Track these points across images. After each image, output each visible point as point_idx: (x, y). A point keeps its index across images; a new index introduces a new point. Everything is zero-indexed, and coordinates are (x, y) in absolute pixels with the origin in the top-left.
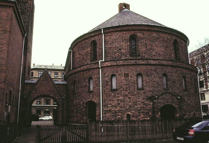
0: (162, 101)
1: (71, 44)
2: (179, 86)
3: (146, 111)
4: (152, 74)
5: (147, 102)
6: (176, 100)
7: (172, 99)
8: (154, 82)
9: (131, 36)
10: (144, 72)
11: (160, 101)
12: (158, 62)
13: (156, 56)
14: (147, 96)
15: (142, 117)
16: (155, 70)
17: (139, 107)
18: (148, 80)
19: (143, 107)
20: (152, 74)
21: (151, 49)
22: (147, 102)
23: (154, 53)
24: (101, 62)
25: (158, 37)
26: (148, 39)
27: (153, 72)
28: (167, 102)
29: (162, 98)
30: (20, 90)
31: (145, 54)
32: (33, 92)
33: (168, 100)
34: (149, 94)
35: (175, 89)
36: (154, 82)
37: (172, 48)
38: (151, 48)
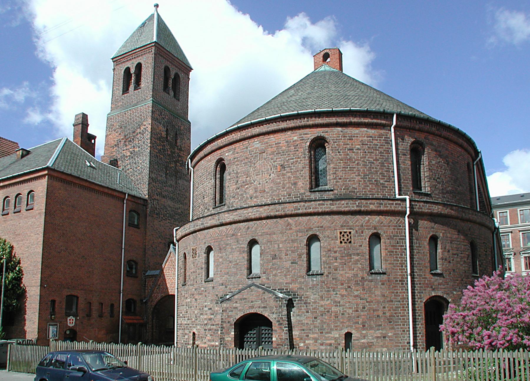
0: (239, 305)
1: (474, 143)
2: (290, 267)
3: (214, 327)
4: (227, 245)
5: (216, 308)
6: (272, 303)
7: (264, 301)
8: (231, 262)
9: (313, 141)
10: (214, 242)
11: (234, 305)
12: (237, 215)
13: (256, 197)
14: (217, 295)
15: (209, 340)
16: (233, 235)
17: (206, 319)
18: (221, 260)
19: (210, 319)
20: (227, 245)
21: (245, 183)
22: (216, 308)
23: (251, 192)
24: (399, 195)
25: (263, 147)
26: (242, 161)
27: (231, 241)
28: (252, 307)
29: (241, 299)
30: (122, 290)
31: (234, 197)
32: (155, 291)
33: (252, 302)
34: (220, 291)
35: (275, 275)
36: (231, 262)
37: (300, 166)
38: (246, 180)
